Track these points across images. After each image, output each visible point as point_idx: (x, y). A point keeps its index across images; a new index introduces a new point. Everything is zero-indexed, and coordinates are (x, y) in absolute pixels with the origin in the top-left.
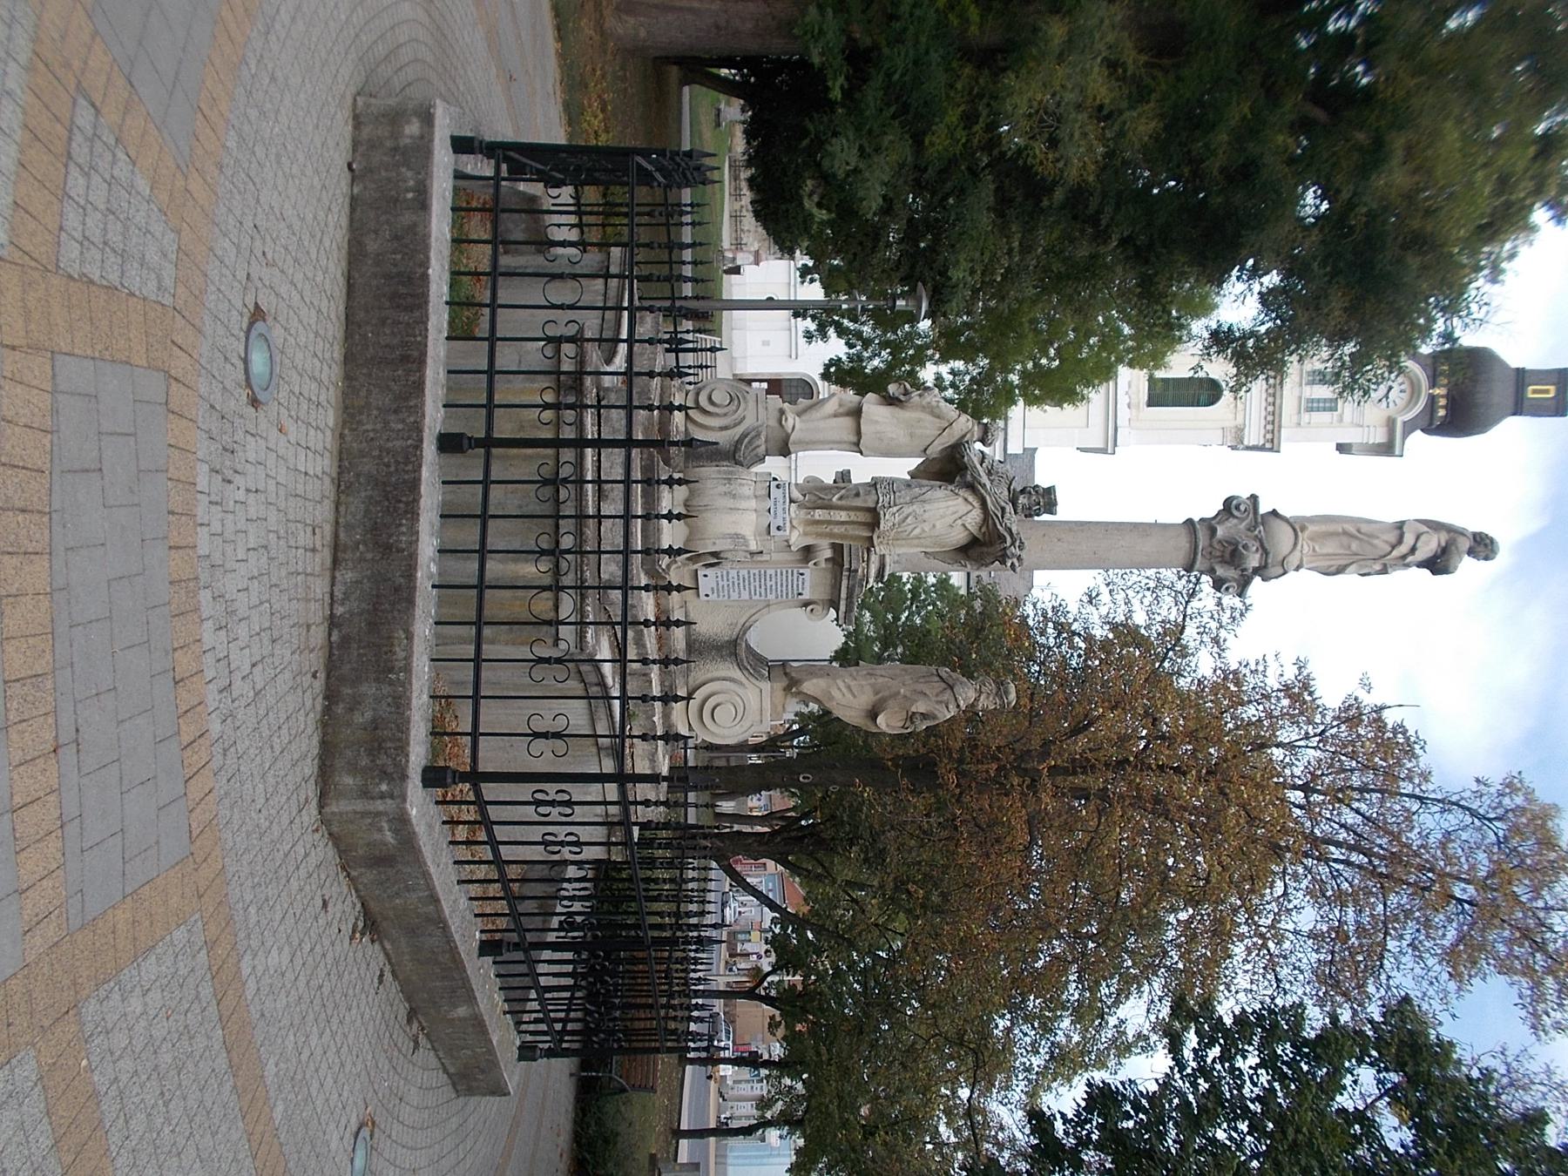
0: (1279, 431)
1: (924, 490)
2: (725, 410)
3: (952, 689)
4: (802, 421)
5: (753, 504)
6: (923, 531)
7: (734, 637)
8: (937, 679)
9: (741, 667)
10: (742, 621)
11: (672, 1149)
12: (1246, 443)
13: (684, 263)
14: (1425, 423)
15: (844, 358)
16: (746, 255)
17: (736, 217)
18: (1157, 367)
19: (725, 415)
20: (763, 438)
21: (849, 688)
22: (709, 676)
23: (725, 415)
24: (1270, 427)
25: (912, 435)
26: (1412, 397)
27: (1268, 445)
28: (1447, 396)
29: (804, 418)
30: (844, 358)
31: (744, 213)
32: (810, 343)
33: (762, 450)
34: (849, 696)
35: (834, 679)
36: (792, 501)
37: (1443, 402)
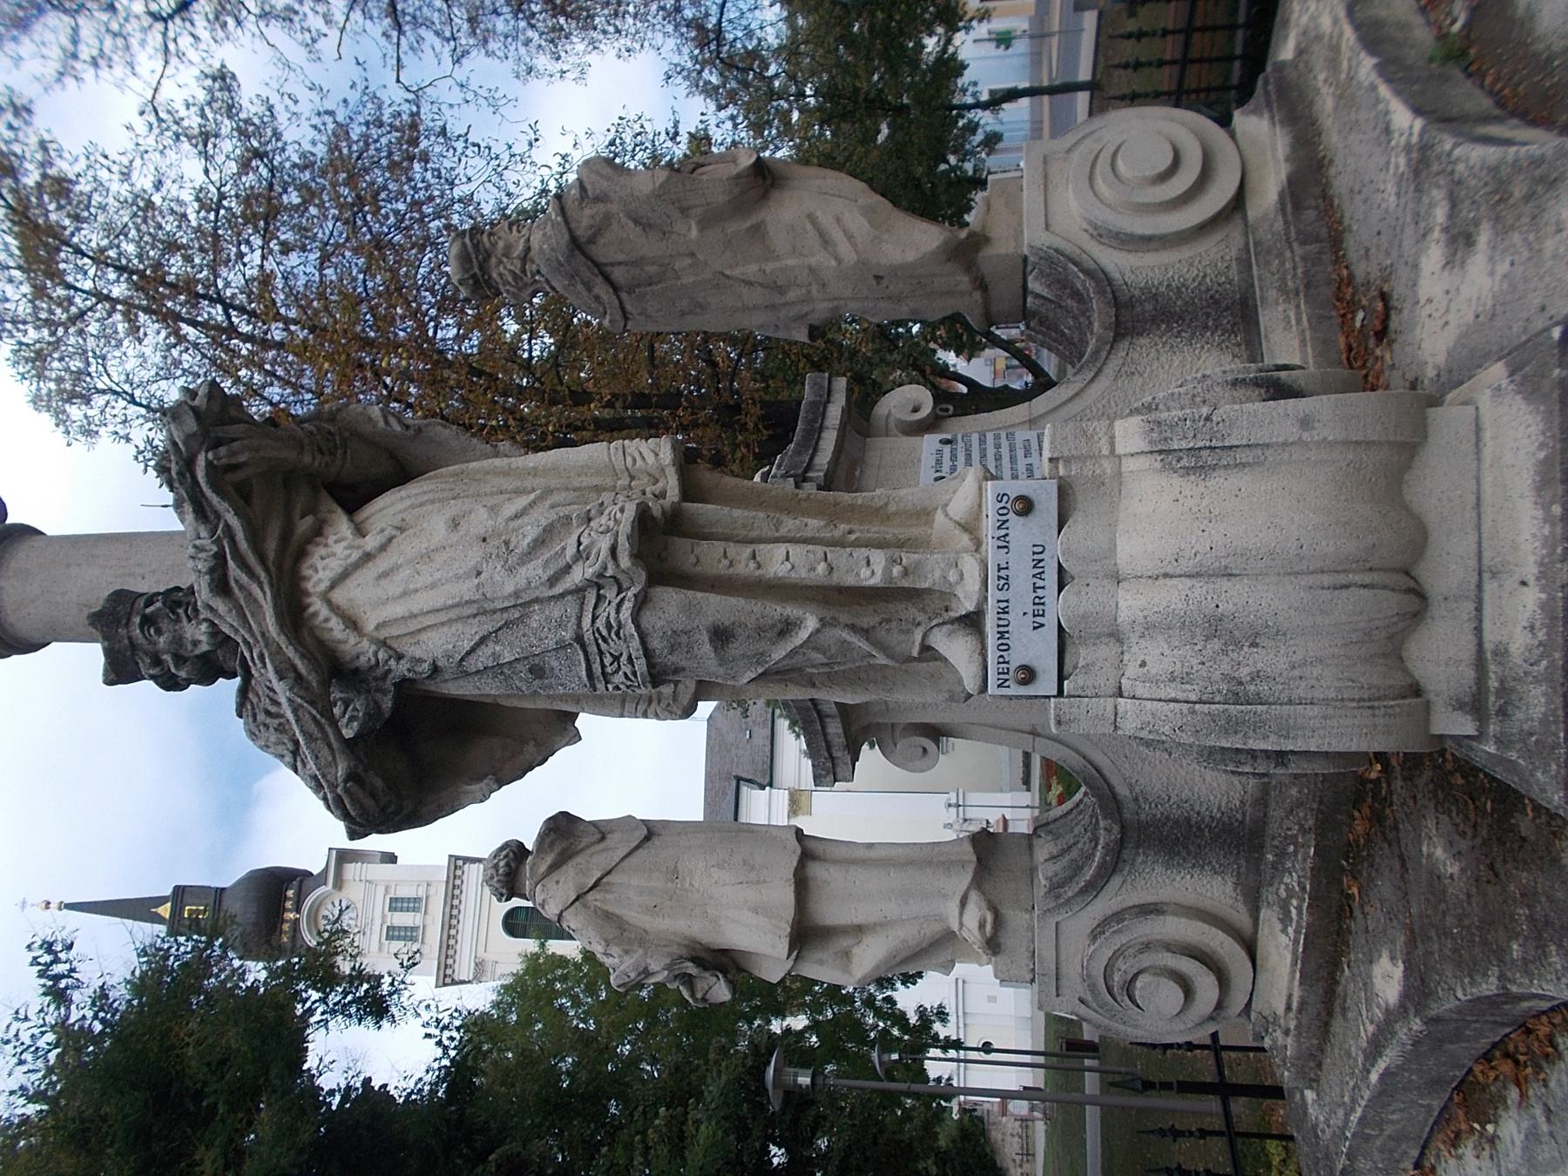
0: (448, 877)
1: (483, 658)
2: (1147, 960)
3: (574, 240)
4: (940, 918)
5: (1130, 604)
6: (493, 510)
7: (1125, 344)
8: (618, 274)
9: (1101, 278)
10: (1103, 383)
11: (1100, 69)
12: (482, 866)
14: (308, 883)
15: (898, 985)
16: (1016, 1112)
17: (1028, 1153)
18: (536, 956)
19: (1147, 946)
20: (1042, 880)
21: (826, 242)
22: (1186, 252)
23: (1147, 946)
24: (458, 882)
25: (674, 874)
26: (317, 910)
27: (460, 863)
28: (285, 910)
29: (933, 929)
30: (898, 985)
31: (1018, 1158)
32: (940, 1006)
33: (1043, 849)
34: (826, 220)
35: (862, 263)
36: (972, 622)
37: (289, 904)
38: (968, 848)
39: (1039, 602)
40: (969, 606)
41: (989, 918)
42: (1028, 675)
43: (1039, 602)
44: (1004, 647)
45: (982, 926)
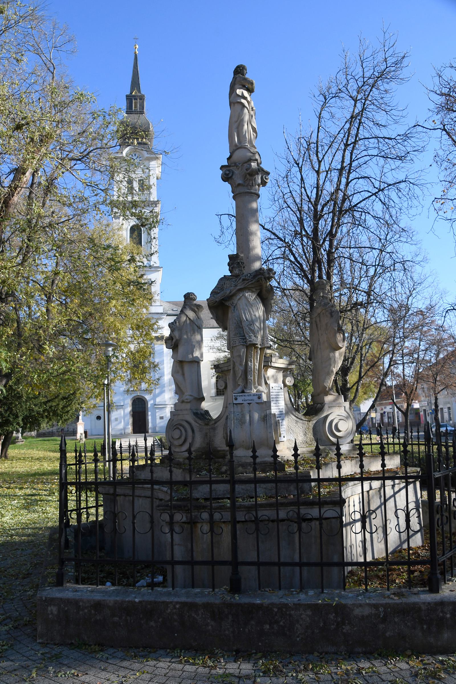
13: (418, 432)
38: (201, 397)
39: (246, 400)
40: (245, 391)
41: (189, 401)
42: (236, 399)
43: (246, 400)
44: (240, 396)
45: (187, 399)
